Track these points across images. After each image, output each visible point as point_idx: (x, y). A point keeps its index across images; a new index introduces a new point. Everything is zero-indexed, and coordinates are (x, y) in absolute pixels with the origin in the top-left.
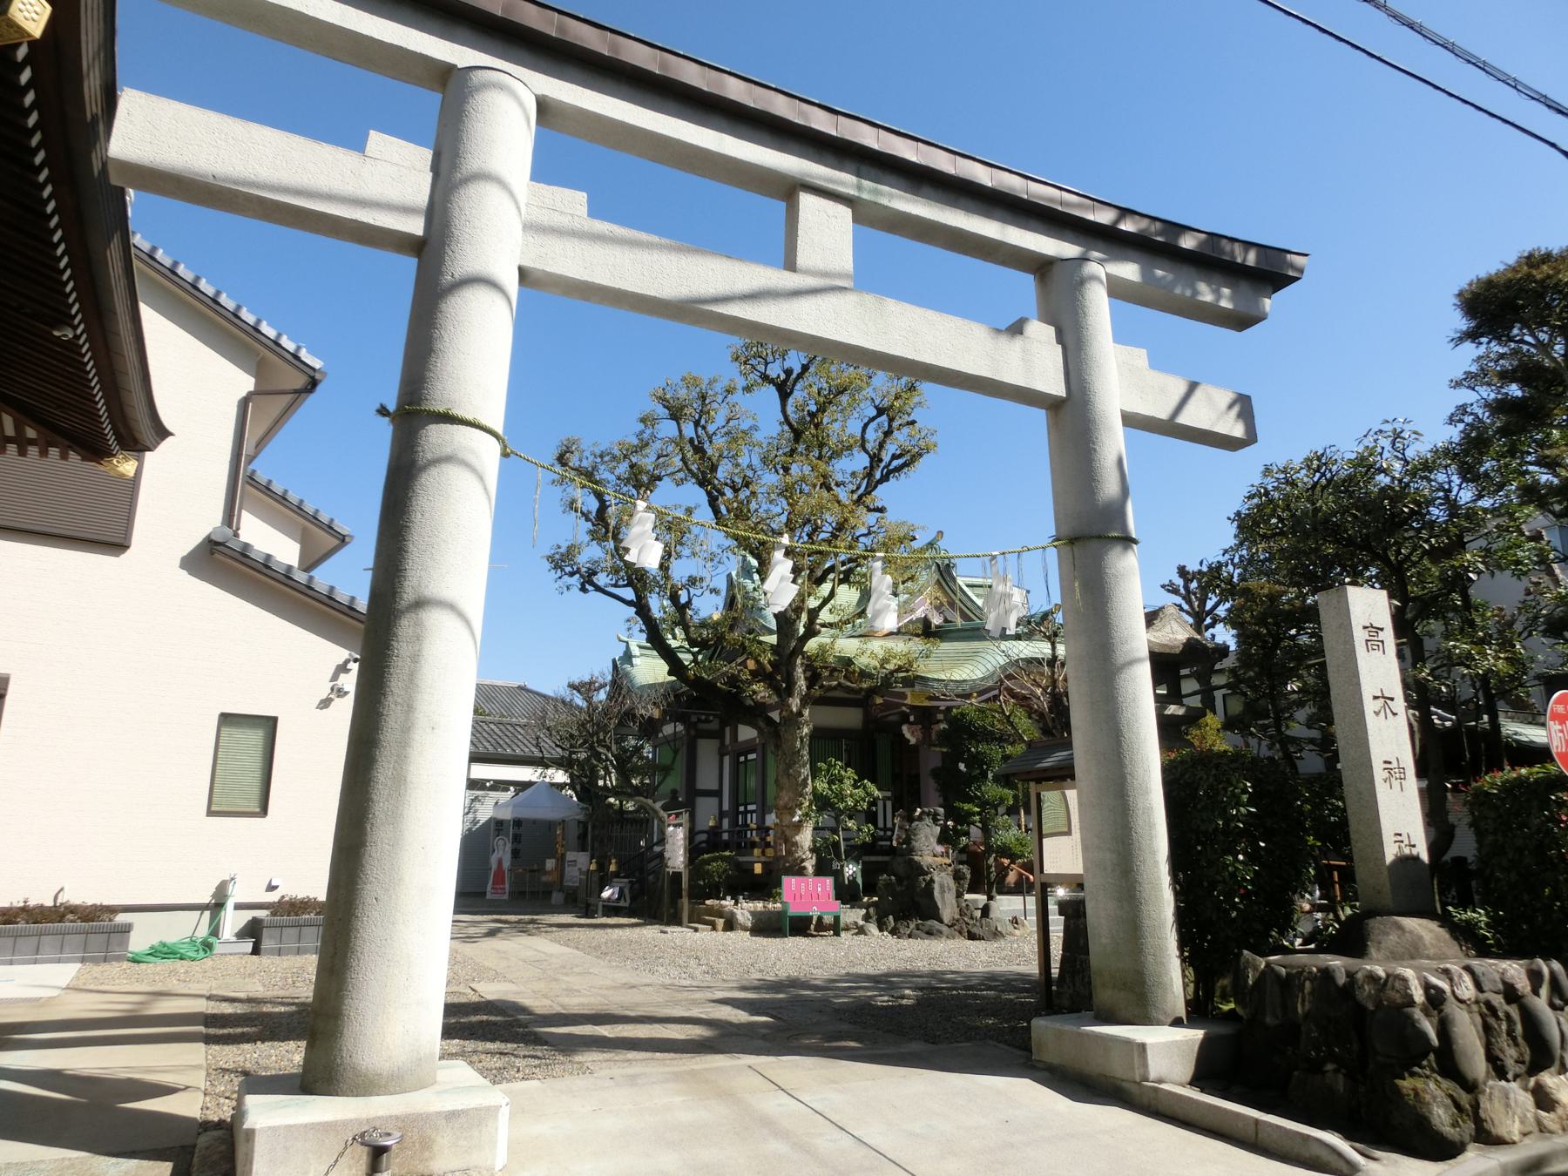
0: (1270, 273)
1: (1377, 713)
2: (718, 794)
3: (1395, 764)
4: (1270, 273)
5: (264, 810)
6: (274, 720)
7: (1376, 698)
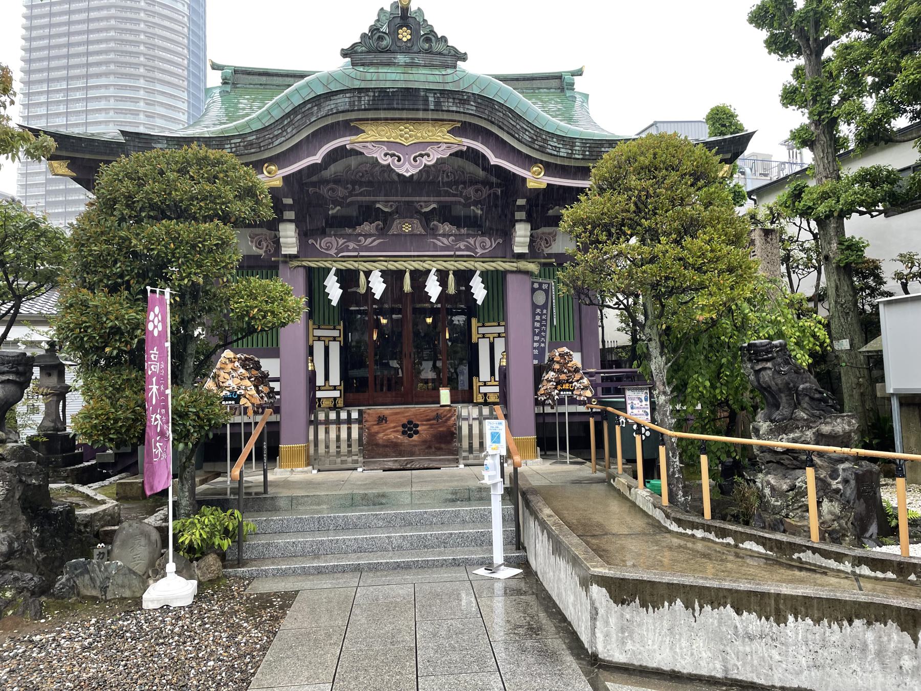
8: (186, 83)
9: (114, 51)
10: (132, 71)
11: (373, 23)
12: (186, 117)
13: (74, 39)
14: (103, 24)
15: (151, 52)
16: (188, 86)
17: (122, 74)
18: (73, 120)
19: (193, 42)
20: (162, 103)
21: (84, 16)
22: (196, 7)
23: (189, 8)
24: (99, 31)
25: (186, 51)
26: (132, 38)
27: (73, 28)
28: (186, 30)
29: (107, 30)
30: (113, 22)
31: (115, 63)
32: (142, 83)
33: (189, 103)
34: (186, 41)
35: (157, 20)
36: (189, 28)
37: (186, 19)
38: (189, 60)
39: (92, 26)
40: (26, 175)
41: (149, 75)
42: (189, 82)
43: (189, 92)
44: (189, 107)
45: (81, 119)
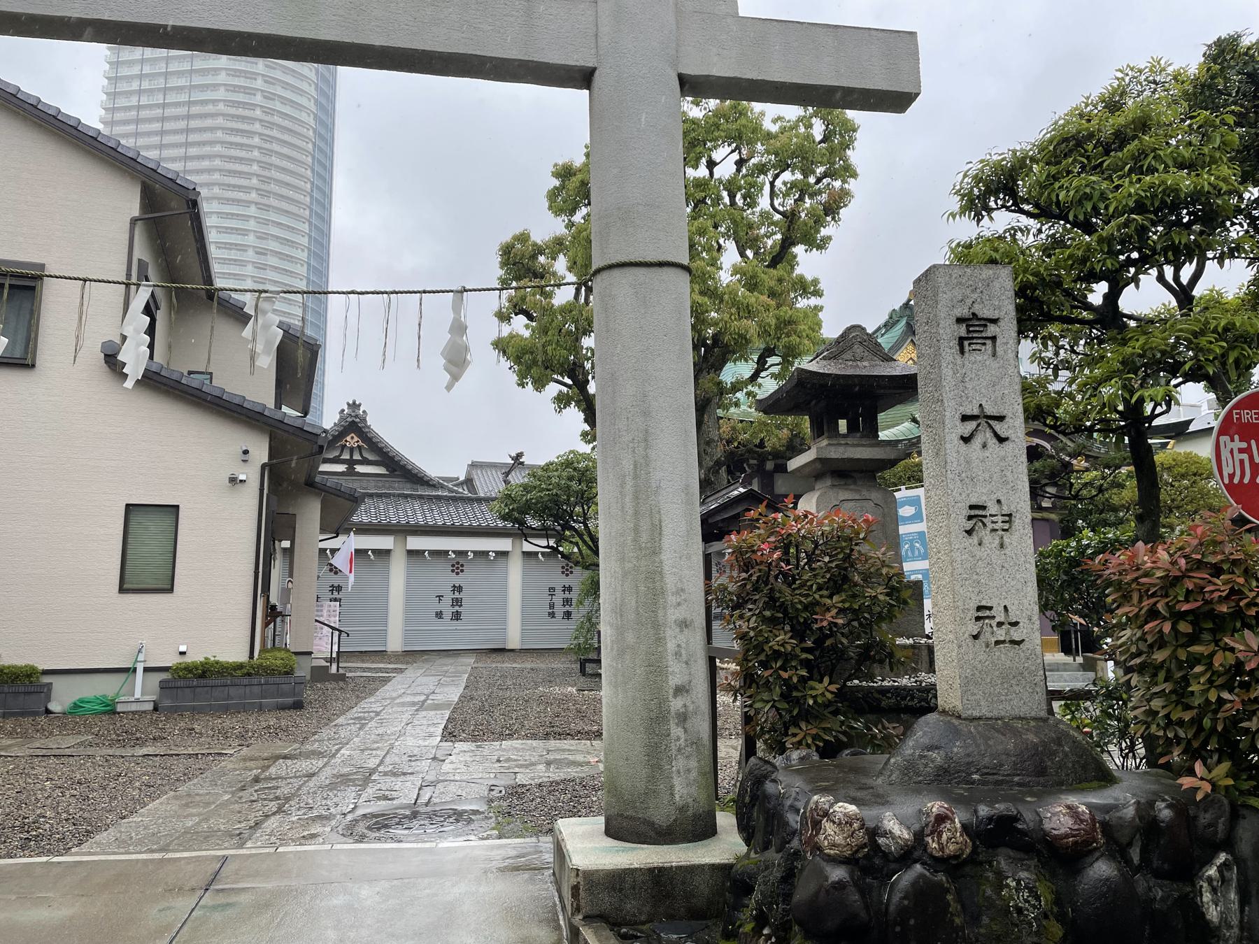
3: (993, 509)
6: (177, 507)
7: (965, 418)
8: (307, 212)
9: (221, 156)
10: (241, 196)
11: (698, 511)
12: (306, 254)
13: (169, 126)
14: (207, 136)
15: (266, 173)
16: (311, 216)
17: (228, 200)
18: (167, 153)
19: (319, 161)
20: (278, 237)
21: (182, 124)
22: (324, 118)
23: (316, 89)
24: (199, 144)
25: (309, 172)
26: (243, 154)
27: (169, 112)
28: (310, 146)
29: (211, 143)
30: (219, 134)
31: (219, 184)
32: (252, 211)
33: (310, 237)
34: (310, 159)
35: (275, 133)
36: (314, 144)
37: (311, 133)
38: (312, 183)
39: (194, 124)
40: (116, 65)
41: (263, 187)
42: (311, 210)
43: (310, 223)
44: (309, 243)
45: (173, 67)
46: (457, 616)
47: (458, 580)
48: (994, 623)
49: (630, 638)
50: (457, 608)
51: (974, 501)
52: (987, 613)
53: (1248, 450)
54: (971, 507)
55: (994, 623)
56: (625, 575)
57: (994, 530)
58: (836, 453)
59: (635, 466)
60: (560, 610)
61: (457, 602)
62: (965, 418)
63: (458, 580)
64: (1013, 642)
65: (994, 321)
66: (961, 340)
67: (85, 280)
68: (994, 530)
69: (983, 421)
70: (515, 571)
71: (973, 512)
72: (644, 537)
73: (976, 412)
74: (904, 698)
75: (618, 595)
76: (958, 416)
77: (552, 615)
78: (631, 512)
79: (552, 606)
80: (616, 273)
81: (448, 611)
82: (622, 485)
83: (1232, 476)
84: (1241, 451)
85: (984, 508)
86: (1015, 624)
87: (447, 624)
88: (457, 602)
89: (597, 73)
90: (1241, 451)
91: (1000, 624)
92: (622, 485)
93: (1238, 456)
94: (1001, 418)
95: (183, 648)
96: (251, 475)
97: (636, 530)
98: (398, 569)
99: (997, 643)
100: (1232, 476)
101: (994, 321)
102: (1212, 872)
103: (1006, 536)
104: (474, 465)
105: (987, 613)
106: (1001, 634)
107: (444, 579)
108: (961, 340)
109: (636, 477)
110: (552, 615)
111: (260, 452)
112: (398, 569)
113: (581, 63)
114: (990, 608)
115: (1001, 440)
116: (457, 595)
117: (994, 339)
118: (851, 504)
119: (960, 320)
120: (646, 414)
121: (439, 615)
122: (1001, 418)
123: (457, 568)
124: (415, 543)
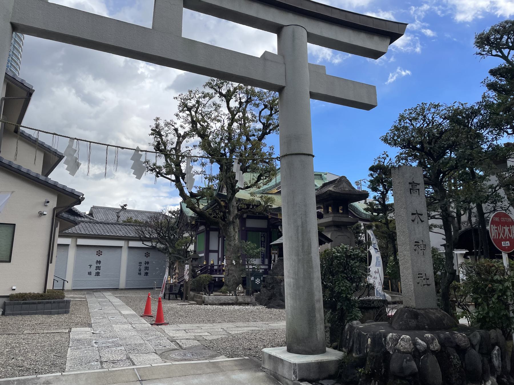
0: (390, 32)
1: (413, 221)
2: (217, 252)
3: (421, 243)
4: (390, 32)
5: (10, 261)
6: (15, 225)
7: (413, 214)
46: (98, 274)
47: (148, 259)
48: (423, 279)
49: (301, 283)
50: (98, 271)
51: (416, 241)
52: (421, 276)
53: (497, 229)
54: (416, 242)
55: (423, 279)
56: (299, 260)
57: (421, 250)
58: (337, 219)
59: (302, 223)
60: (143, 272)
61: (98, 268)
62: (413, 214)
63: (98, 258)
64: (428, 285)
65: (419, 184)
66: (411, 189)
67: (108, 145)
68: (421, 250)
69: (417, 215)
70: (125, 254)
71: (416, 244)
72: (306, 248)
73: (415, 212)
74: (364, 304)
75: (296, 268)
76: (411, 214)
77: (140, 274)
78: (301, 239)
79: (140, 270)
80: (294, 157)
81: (94, 272)
82: (297, 230)
83: (494, 236)
84: (496, 229)
85: (418, 242)
86: (428, 279)
87: (93, 277)
88: (98, 268)
89: (286, 88)
90: (496, 229)
91: (424, 279)
92: (297, 230)
93: (495, 231)
94: (421, 215)
95: (14, 288)
96: (48, 211)
97: (303, 246)
98: (72, 252)
99: (424, 285)
100: (494, 236)
101: (419, 184)
102: (496, 352)
103: (425, 251)
104: (94, 207)
105: (421, 276)
106: (424, 282)
107: (92, 257)
108: (411, 189)
109: (302, 227)
110: (140, 274)
111: (53, 203)
112: (72, 252)
113: (281, 84)
114: (421, 274)
115: (422, 221)
116: (98, 265)
117: (419, 190)
118: (341, 237)
119: (410, 183)
120: (305, 205)
121: (90, 273)
122: (421, 215)
123: (99, 254)
124: (81, 242)
